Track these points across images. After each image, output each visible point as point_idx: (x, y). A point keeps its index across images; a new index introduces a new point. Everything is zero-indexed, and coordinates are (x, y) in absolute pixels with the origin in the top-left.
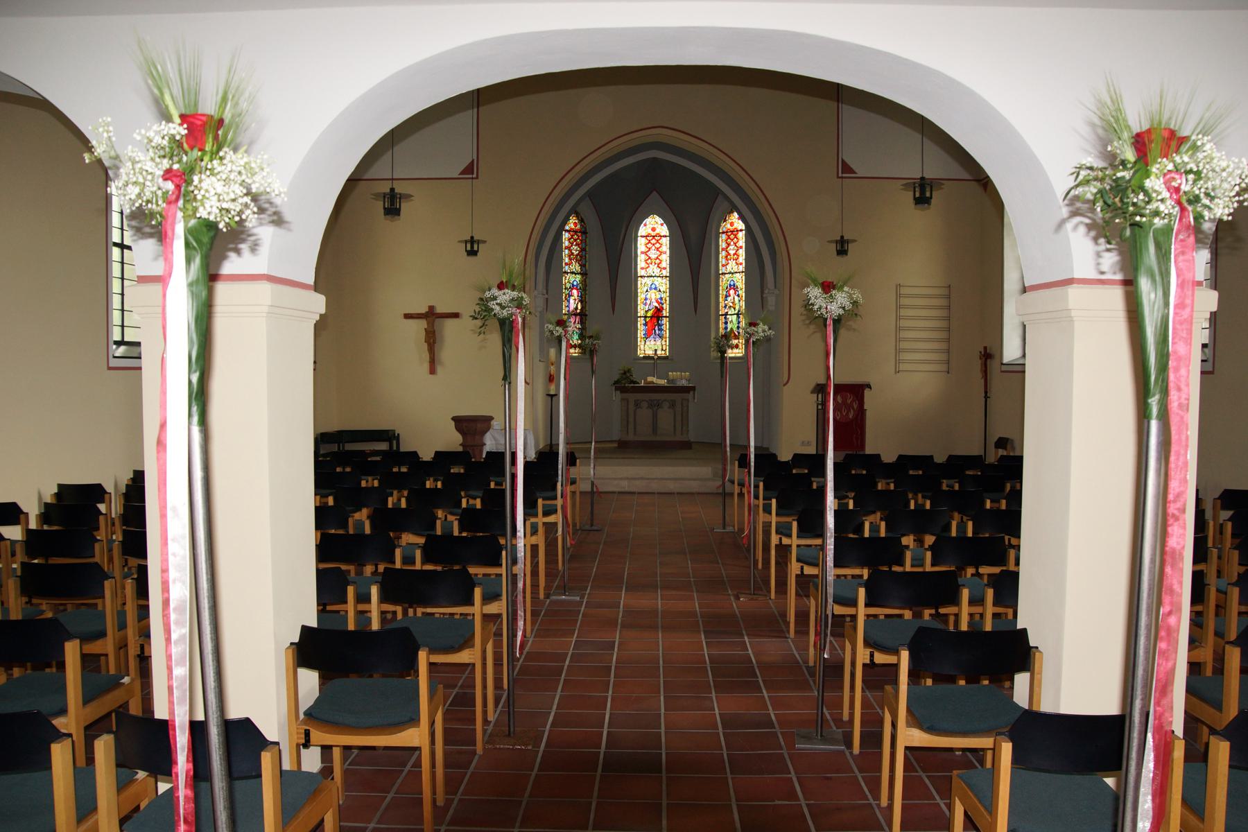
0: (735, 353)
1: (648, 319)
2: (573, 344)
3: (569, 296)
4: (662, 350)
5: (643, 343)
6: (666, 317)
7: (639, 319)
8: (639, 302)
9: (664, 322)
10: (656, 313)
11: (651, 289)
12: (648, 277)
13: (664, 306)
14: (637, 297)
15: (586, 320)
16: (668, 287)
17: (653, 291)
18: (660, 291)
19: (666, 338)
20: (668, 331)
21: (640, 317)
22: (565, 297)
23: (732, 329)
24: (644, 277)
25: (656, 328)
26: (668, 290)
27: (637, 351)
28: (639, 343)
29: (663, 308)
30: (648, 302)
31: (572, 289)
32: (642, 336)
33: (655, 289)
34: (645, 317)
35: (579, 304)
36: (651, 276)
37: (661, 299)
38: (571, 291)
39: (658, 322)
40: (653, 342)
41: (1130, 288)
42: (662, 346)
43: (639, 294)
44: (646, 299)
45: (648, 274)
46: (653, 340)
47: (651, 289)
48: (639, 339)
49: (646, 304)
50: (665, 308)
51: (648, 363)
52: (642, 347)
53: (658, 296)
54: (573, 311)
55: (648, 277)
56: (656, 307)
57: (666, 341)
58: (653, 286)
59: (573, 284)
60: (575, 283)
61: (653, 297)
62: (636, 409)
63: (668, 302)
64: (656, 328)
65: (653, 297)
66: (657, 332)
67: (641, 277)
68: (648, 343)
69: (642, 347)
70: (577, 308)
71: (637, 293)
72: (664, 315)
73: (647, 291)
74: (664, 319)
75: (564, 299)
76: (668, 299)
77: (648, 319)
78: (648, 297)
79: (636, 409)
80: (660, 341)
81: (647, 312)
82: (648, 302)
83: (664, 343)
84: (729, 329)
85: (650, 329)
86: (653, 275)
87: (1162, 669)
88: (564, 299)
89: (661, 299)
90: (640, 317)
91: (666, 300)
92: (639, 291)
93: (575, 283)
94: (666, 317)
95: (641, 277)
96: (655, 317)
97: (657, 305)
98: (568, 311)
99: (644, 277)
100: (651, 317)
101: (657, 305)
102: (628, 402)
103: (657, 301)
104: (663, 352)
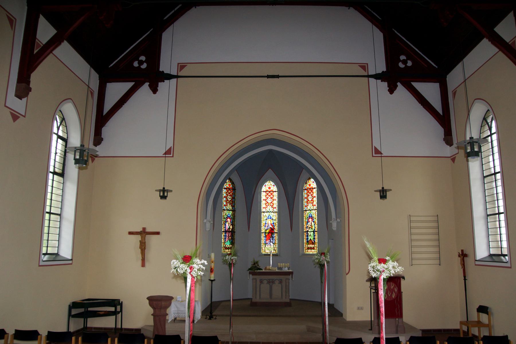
0: (313, 252)
1: (267, 234)
3: (226, 222)
4: (274, 250)
5: (264, 246)
6: (276, 233)
8: (262, 225)
10: (271, 231)
11: (268, 218)
12: (267, 212)
13: (275, 227)
17: (270, 219)
18: (273, 219)
19: (276, 244)
20: (277, 240)
21: (263, 233)
22: (224, 223)
23: (310, 239)
24: (265, 212)
25: (271, 239)
29: (274, 228)
32: (264, 243)
33: (271, 218)
34: (265, 233)
36: (268, 212)
37: (274, 223)
39: (272, 235)
40: (269, 246)
42: (274, 248)
44: (266, 224)
45: (267, 211)
47: (268, 218)
48: (262, 245)
49: (265, 226)
52: (264, 248)
53: (272, 222)
54: (228, 230)
55: (267, 212)
56: (271, 228)
57: (276, 245)
58: (269, 217)
60: (229, 215)
61: (269, 222)
64: (271, 239)
65: (269, 222)
66: (271, 240)
67: (263, 212)
68: (267, 246)
69: (264, 248)
72: (275, 232)
73: (266, 219)
76: (277, 223)
77: (267, 234)
78: (267, 222)
81: (266, 230)
82: (267, 225)
83: (275, 246)
84: (309, 239)
86: (270, 211)
89: (274, 223)
90: (263, 233)
91: (276, 224)
92: (262, 219)
93: (229, 215)
94: (276, 233)
95: (263, 212)
96: (270, 233)
97: (271, 227)
99: (265, 212)
100: (268, 233)
102: (256, 281)
103: (271, 225)
104: (275, 251)
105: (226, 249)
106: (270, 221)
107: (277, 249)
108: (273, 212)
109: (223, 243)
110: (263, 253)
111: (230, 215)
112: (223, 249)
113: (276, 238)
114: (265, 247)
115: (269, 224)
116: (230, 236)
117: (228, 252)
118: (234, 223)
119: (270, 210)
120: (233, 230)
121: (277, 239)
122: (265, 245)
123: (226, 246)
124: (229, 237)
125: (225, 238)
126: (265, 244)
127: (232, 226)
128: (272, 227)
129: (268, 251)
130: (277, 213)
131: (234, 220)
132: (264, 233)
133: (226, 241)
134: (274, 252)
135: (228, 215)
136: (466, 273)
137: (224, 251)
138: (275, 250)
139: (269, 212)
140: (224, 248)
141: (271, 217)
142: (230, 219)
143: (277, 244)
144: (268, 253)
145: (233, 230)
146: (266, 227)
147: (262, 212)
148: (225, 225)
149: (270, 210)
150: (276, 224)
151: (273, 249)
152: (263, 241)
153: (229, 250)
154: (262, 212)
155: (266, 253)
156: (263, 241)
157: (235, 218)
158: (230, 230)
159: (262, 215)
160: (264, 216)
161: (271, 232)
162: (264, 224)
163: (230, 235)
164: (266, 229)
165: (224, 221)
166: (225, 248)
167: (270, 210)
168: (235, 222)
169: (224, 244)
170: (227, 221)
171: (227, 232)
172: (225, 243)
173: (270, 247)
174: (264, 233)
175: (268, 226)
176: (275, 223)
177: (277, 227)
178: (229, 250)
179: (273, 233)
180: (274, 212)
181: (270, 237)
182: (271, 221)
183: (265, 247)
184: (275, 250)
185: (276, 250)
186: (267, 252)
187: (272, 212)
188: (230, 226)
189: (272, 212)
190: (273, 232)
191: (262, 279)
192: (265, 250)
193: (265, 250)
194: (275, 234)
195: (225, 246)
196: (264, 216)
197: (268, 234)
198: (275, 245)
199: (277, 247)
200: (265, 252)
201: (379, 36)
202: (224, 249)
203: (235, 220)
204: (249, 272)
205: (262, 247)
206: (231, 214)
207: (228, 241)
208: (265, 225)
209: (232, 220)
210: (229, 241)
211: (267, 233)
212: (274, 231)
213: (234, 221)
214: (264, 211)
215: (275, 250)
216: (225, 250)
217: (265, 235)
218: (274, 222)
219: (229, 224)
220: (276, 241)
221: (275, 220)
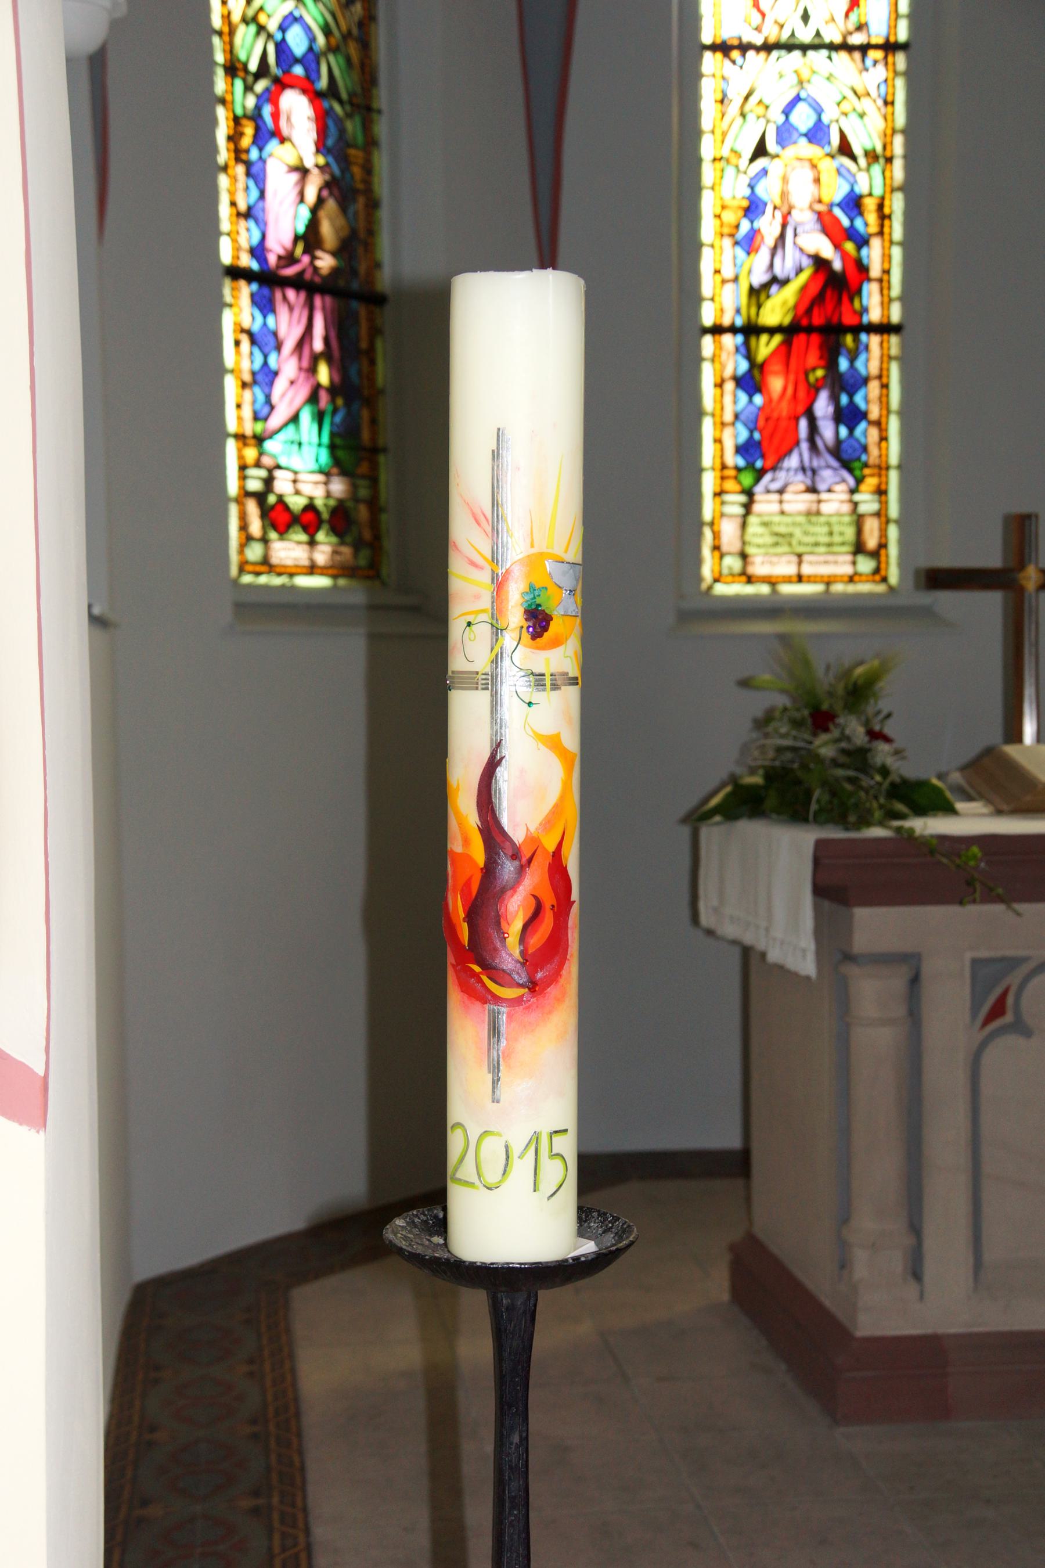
1: (766, 347)
2: (297, 503)
3: (260, 139)
4: (859, 548)
5: (735, 502)
6: (884, 329)
7: (707, 343)
8: (708, 230)
9: (870, 362)
10: (818, 300)
11: (785, 134)
12: (767, 48)
13: (873, 255)
14: (696, 189)
15: (375, 331)
16: (900, 119)
17: (804, 148)
18: (845, 149)
19: (882, 469)
20: (894, 426)
21: (717, 330)
22: (234, 138)
24: (744, 48)
25: (823, 406)
26: (898, 145)
27: (698, 561)
28: (708, 509)
29: (862, 269)
30: (769, 226)
31: (281, 84)
32: (732, 459)
33: (817, 134)
34: (751, 330)
35: (331, 204)
36: (789, 47)
37: (854, 203)
38: (272, 97)
39: (831, 365)
40: (798, 501)
41: (795, 579)
42: (859, 521)
43: (708, 174)
44: (753, 208)
45: (771, 33)
46: (799, 482)
47: (785, 134)
48: (709, 482)
49: (750, 243)
50: (875, 272)
51: (753, 636)
52: (729, 530)
53: (835, 191)
54: (289, 259)
55: (767, 48)
56: (820, 263)
57: (881, 492)
58: (803, 119)
59: (282, 47)
60: (297, 42)
61: (802, 195)
62: (983, 1045)
63: (897, 230)
64: (823, 406)
65: (802, 195)
66: (827, 431)
67: (723, 48)
68: (765, 505)
69: (729, 530)
70: (310, 239)
71: (698, 162)
72: (875, 315)
73: (761, 150)
74: (874, 341)
75: (224, 155)
76: (897, 204)
77: (766, 347)
78: (768, 191)
79: (983, 1045)
80: (841, 492)
81: (758, 294)
82: (769, 226)
83: (868, 503)
85: (784, 409)
86: (805, 36)
87: (490, 997)
88: (224, 155)
89: (854, 203)
90: (717, 330)
91: (883, 217)
92: (707, 148)
93: (297, 42)
94: (884, 329)
95: (723, 48)
96: (809, 330)
97: (827, 250)
98: (258, 251)
99: (744, 48)
100: (789, 331)
101: (827, 250)
102: (915, 980)
103: (827, 224)
104: (865, 565)
105: (282, 531)
106: (810, 175)
107: (893, 532)
108: (845, 47)
109: (240, 437)
110: (720, 589)
111: (308, 29)
112: (244, 527)
113: (884, 400)
114: (748, 507)
115: (804, 217)
116: (327, 355)
117: (312, 569)
118: (368, 169)
119: (805, 17)
120: (354, 272)
121: (902, 413)
122: (749, 493)
123: (282, 484)
124: (312, 370)
125: (265, 377)
126: (747, 479)
127: (343, 205)
128: (837, 246)
129: (786, 567)
130: (900, 60)
131: (367, 126)
132: (733, 330)
133: (275, 421)
134: (851, 579)
135: (283, 28)
136: (447, 765)
137: (255, 552)
138: (872, 543)
139: (804, 48)
140: (252, 508)
141: (819, 111)
142: (315, 96)
143: (894, 477)
144: (786, 589)
145: (362, 268)
146: (762, 257)
147: (714, 48)
148: (256, 174)
149: (805, 17)
150: (883, 217)
151: (850, 533)
152: (718, 441)
153: (312, 543)
154: (714, 48)
155: (764, 589)
156: (718, 441)
157: (382, 98)
158: (325, 262)
159: (708, 90)
160: (733, 109)
161: (818, 320)
162: (729, 217)
163: (326, 340)
164: (759, 278)
165: (236, 120)
166: (266, 512)
167: (813, 24)
168: (381, 161)
169: (251, 454)
170: (276, 116)
171: (285, 283)
172: (259, 440)
173: (809, 514)
174: (733, 330)
175: (782, 237)
176: (870, 204)
177: (897, 253)
178: (312, 543)
179: (842, 329)
180: (864, 49)
181: (813, 392)
182: (828, 167)
183: (748, 507)
184: (872, 543)
185: (883, 546)
186: (772, 581)
187: (832, 47)
188: (320, 201)
189: (832, 47)
190: (848, 320)
191: (1014, 963)
192: (744, 556)
193: (744, 556)
194: (874, 340)
195: (269, 481)
196: (733, 109)
197: (787, 344)
198: (871, 482)
199: (894, 511)
200: (750, 580)
201: (454, 278)
202: (256, 527)
203: (382, 128)
204: (819, 844)
205: (707, 514)
206: (327, 31)
207: (295, 419)
208: (745, 226)
209: (342, 131)
210: (320, 417)
211: (772, 331)
212: (865, 310)
213: (371, 143)
214: (728, 33)
215: (875, 554)
216: (265, 540)
217: (749, 355)
218: (862, 188)
219: (302, 171)
220: (883, 438)
221: (872, 156)
